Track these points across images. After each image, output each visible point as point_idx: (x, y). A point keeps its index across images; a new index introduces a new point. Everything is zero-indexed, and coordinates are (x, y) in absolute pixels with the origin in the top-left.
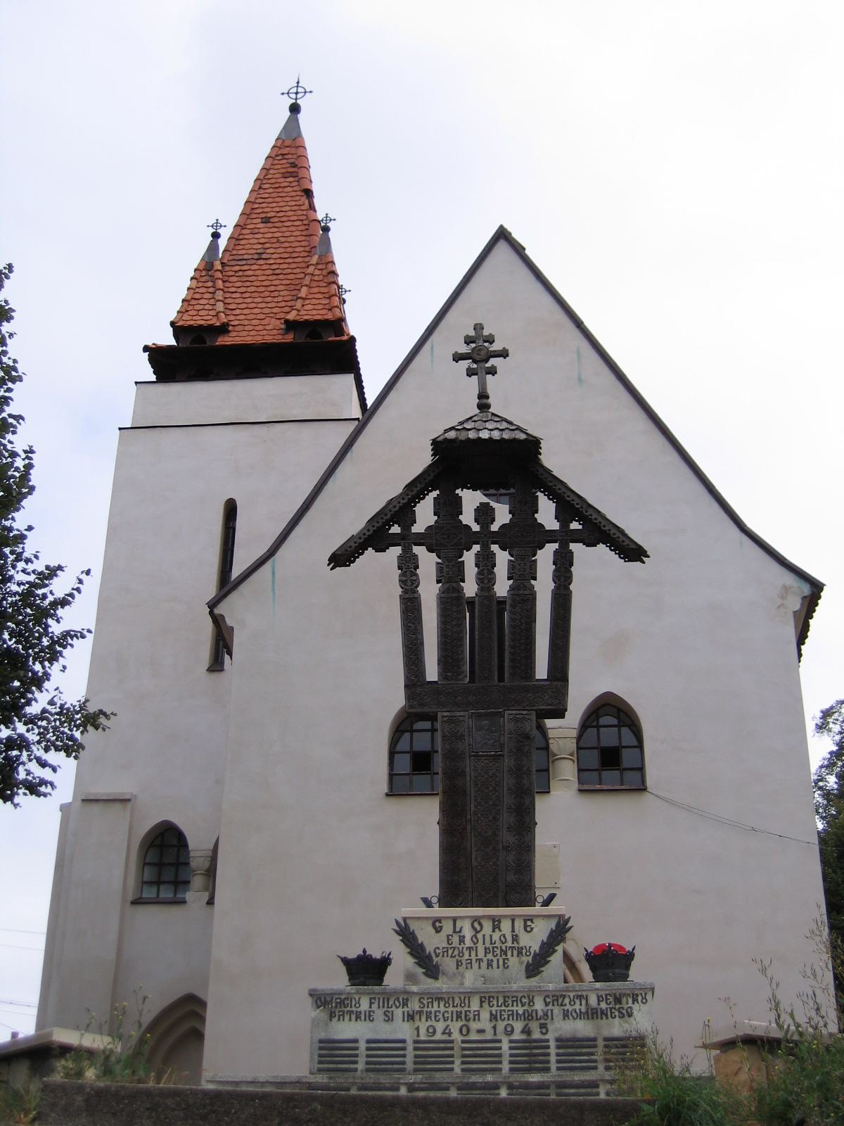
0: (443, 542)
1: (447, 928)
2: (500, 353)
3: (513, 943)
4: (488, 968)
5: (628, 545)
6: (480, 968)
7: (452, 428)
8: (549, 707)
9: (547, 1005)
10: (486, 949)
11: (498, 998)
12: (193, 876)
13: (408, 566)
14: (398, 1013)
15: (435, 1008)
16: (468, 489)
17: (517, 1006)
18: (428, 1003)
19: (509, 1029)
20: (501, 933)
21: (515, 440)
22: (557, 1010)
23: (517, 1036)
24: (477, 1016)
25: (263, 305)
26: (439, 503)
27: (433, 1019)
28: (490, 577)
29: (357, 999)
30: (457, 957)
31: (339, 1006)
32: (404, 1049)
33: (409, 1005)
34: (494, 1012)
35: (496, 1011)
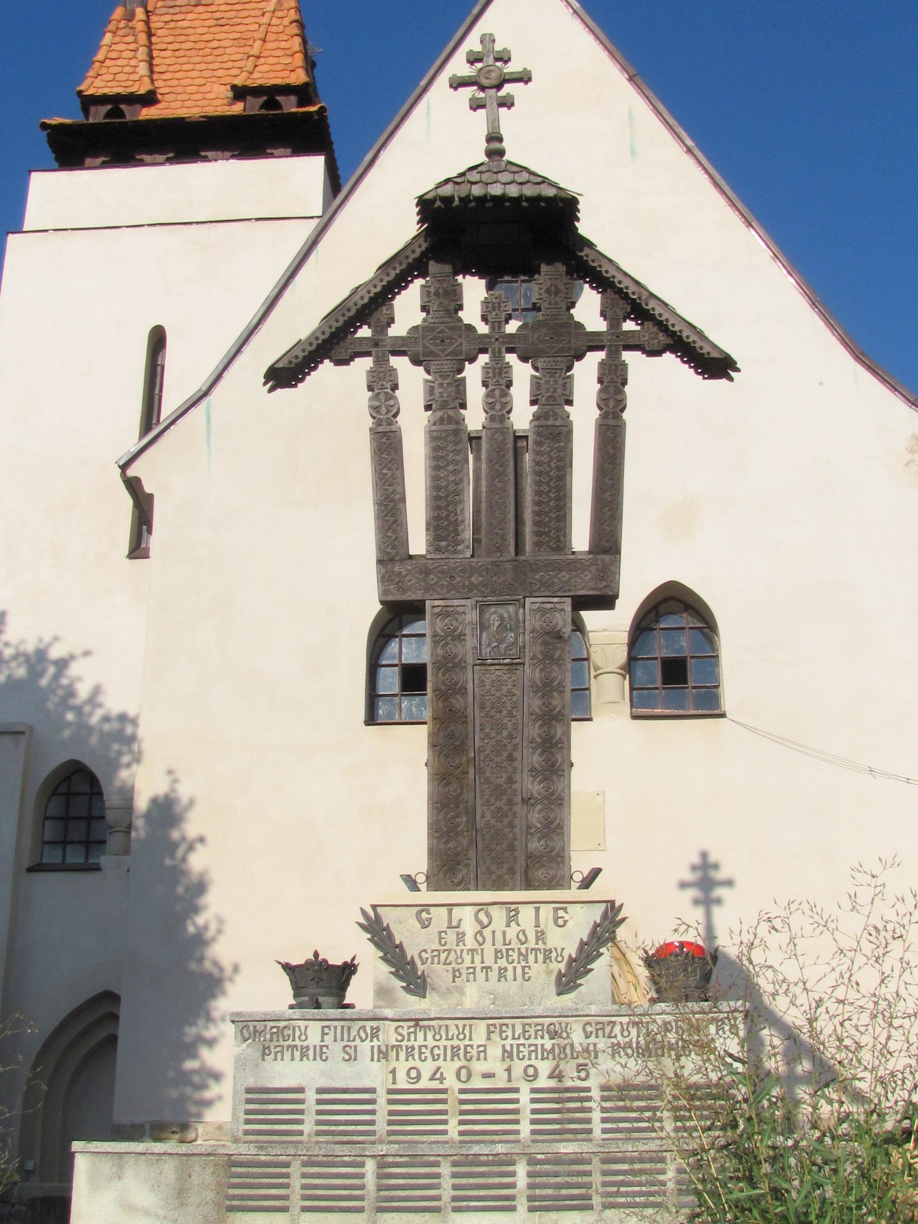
0: (434, 349)
1: (439, 916)
2: (519, 76)
3: (537, 944)
4: (499, 981)
5: (708, 353)
6: (487, 980)
7: (447, 181)
8: (591, 593)
9: (587, 1036)
10: (496, 951)
11: (513, 1026)
12: (111, 833)
13: (382, 385)
14: (365, 1047)
15: (420, 1041)
16: (473, 275)
17: (542, 1037)
18: (409, 1034)
19: (531, 1071)
20: (520, 928)
21: (539, 198)
22: (602, 1043)
23: (543, 1082)
24: (483, 1051)
25: (203, 66)
26: (429, 293)
27: (416, 1057)
28: (504, 400)
29: (303, 1029)
30: (454, 965)
31: (275, 1037)
32: (372, 1102)
33: (381, 1037)
34: (508, 1048)
35: (512, 1045)
